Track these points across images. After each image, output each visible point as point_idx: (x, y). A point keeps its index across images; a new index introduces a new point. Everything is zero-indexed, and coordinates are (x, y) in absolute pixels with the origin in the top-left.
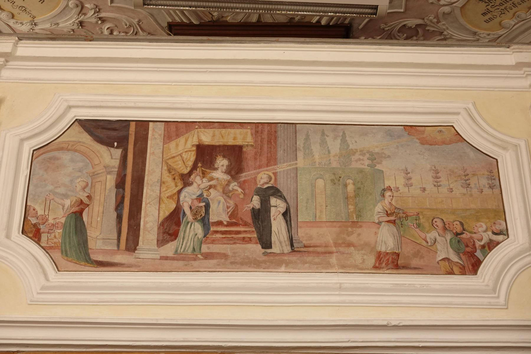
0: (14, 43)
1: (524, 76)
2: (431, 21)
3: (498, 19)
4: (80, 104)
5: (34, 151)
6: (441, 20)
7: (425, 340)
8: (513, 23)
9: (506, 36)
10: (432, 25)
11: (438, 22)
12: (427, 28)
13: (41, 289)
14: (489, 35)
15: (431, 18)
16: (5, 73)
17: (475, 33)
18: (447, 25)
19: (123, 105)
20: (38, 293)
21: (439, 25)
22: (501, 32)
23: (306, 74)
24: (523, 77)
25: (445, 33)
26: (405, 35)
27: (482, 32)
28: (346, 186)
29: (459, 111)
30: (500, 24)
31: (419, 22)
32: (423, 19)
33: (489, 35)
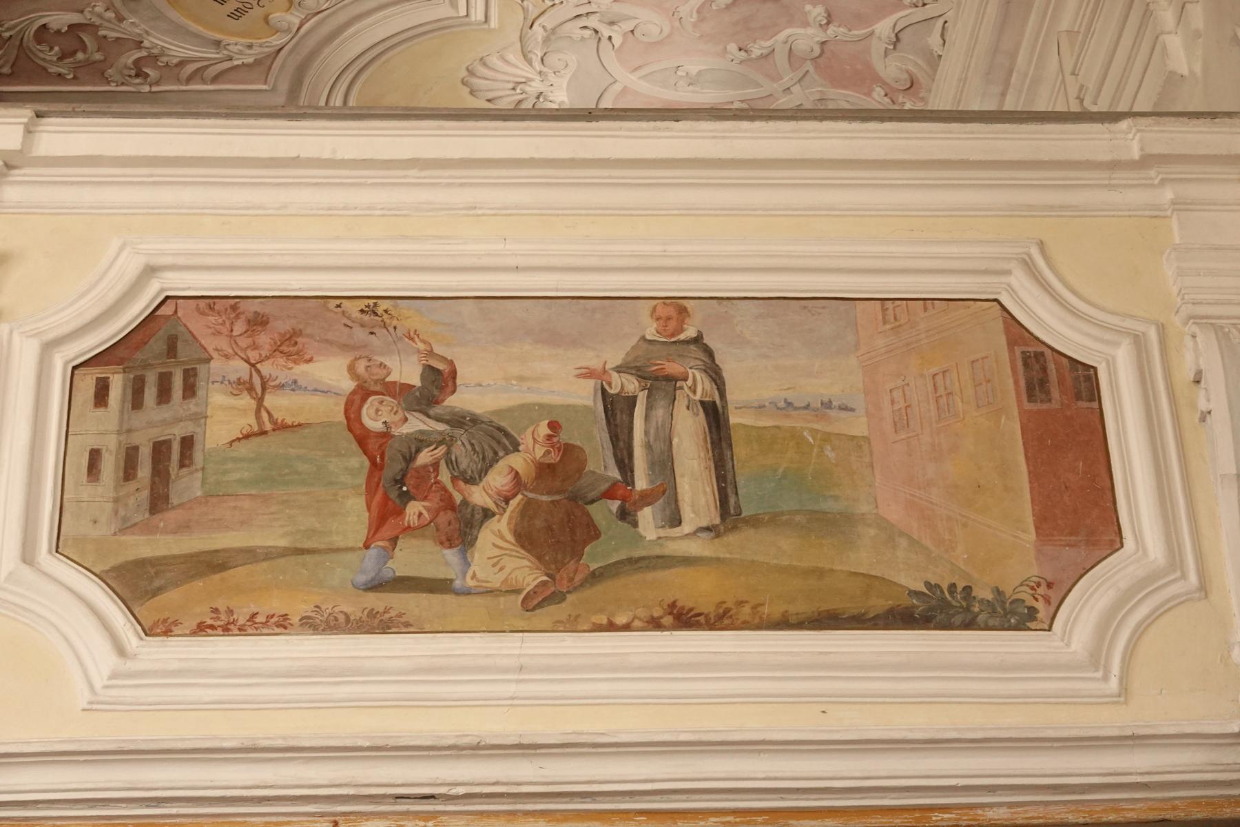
0: (26, 125)
1: (1156, 182)
2: (100, 16)
3: (257, 12)
4: (181, 261)
5: (74, 368)
6: (125, 13)
7: (132, 747)
8: (297, 21)
9: (291, 51)
10: (106, 24)
11: (121, 19)
12: (102, 33)
13: (110, 678)
14: (250, 46)
15: (97, 9)
16: (12, 194)
17: (218, 43)
18: (143, 26)
19: (266, 261)
20: (107, 687)
21: (125, 24)
22: (276, 41)
23: (685, 185)
24: (1152, 186)
25: (146, 44)
26: (56, 48)
27: (233, 40)
28: (833, 449)
29: (1006, 266)
30: (266, 20)
31: (75, 18)
32: (82, 12)
33: (250, 46)
